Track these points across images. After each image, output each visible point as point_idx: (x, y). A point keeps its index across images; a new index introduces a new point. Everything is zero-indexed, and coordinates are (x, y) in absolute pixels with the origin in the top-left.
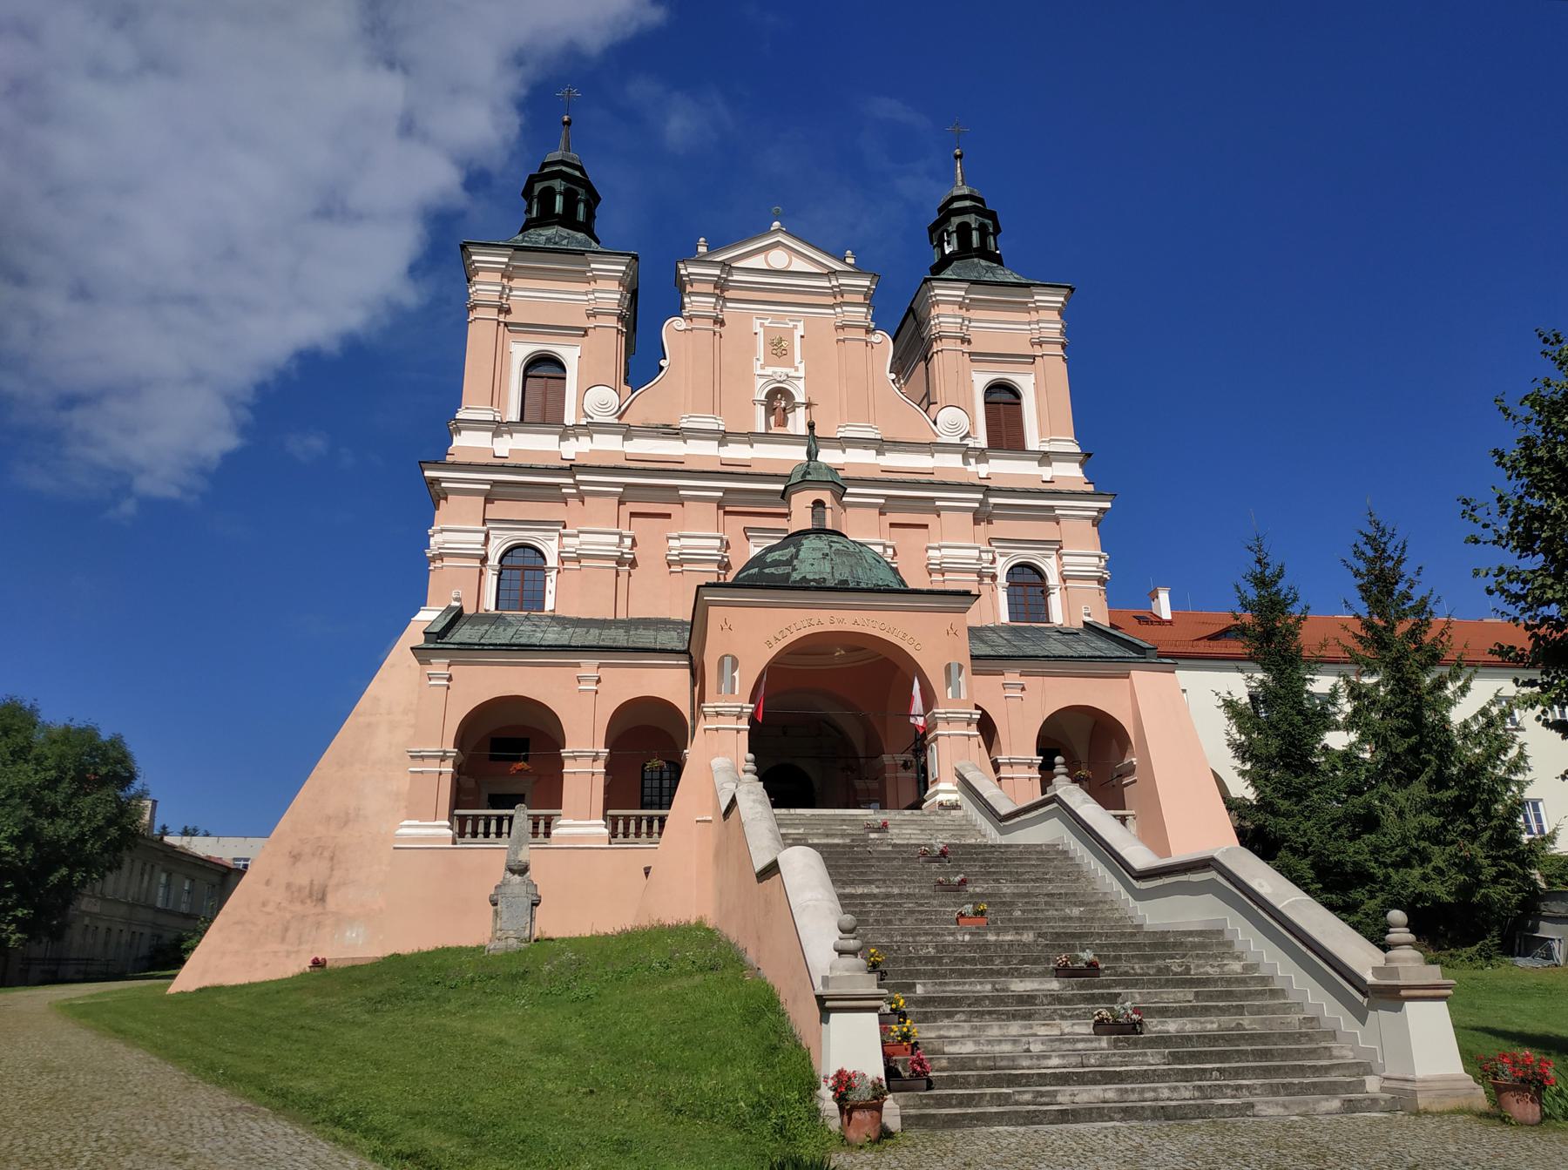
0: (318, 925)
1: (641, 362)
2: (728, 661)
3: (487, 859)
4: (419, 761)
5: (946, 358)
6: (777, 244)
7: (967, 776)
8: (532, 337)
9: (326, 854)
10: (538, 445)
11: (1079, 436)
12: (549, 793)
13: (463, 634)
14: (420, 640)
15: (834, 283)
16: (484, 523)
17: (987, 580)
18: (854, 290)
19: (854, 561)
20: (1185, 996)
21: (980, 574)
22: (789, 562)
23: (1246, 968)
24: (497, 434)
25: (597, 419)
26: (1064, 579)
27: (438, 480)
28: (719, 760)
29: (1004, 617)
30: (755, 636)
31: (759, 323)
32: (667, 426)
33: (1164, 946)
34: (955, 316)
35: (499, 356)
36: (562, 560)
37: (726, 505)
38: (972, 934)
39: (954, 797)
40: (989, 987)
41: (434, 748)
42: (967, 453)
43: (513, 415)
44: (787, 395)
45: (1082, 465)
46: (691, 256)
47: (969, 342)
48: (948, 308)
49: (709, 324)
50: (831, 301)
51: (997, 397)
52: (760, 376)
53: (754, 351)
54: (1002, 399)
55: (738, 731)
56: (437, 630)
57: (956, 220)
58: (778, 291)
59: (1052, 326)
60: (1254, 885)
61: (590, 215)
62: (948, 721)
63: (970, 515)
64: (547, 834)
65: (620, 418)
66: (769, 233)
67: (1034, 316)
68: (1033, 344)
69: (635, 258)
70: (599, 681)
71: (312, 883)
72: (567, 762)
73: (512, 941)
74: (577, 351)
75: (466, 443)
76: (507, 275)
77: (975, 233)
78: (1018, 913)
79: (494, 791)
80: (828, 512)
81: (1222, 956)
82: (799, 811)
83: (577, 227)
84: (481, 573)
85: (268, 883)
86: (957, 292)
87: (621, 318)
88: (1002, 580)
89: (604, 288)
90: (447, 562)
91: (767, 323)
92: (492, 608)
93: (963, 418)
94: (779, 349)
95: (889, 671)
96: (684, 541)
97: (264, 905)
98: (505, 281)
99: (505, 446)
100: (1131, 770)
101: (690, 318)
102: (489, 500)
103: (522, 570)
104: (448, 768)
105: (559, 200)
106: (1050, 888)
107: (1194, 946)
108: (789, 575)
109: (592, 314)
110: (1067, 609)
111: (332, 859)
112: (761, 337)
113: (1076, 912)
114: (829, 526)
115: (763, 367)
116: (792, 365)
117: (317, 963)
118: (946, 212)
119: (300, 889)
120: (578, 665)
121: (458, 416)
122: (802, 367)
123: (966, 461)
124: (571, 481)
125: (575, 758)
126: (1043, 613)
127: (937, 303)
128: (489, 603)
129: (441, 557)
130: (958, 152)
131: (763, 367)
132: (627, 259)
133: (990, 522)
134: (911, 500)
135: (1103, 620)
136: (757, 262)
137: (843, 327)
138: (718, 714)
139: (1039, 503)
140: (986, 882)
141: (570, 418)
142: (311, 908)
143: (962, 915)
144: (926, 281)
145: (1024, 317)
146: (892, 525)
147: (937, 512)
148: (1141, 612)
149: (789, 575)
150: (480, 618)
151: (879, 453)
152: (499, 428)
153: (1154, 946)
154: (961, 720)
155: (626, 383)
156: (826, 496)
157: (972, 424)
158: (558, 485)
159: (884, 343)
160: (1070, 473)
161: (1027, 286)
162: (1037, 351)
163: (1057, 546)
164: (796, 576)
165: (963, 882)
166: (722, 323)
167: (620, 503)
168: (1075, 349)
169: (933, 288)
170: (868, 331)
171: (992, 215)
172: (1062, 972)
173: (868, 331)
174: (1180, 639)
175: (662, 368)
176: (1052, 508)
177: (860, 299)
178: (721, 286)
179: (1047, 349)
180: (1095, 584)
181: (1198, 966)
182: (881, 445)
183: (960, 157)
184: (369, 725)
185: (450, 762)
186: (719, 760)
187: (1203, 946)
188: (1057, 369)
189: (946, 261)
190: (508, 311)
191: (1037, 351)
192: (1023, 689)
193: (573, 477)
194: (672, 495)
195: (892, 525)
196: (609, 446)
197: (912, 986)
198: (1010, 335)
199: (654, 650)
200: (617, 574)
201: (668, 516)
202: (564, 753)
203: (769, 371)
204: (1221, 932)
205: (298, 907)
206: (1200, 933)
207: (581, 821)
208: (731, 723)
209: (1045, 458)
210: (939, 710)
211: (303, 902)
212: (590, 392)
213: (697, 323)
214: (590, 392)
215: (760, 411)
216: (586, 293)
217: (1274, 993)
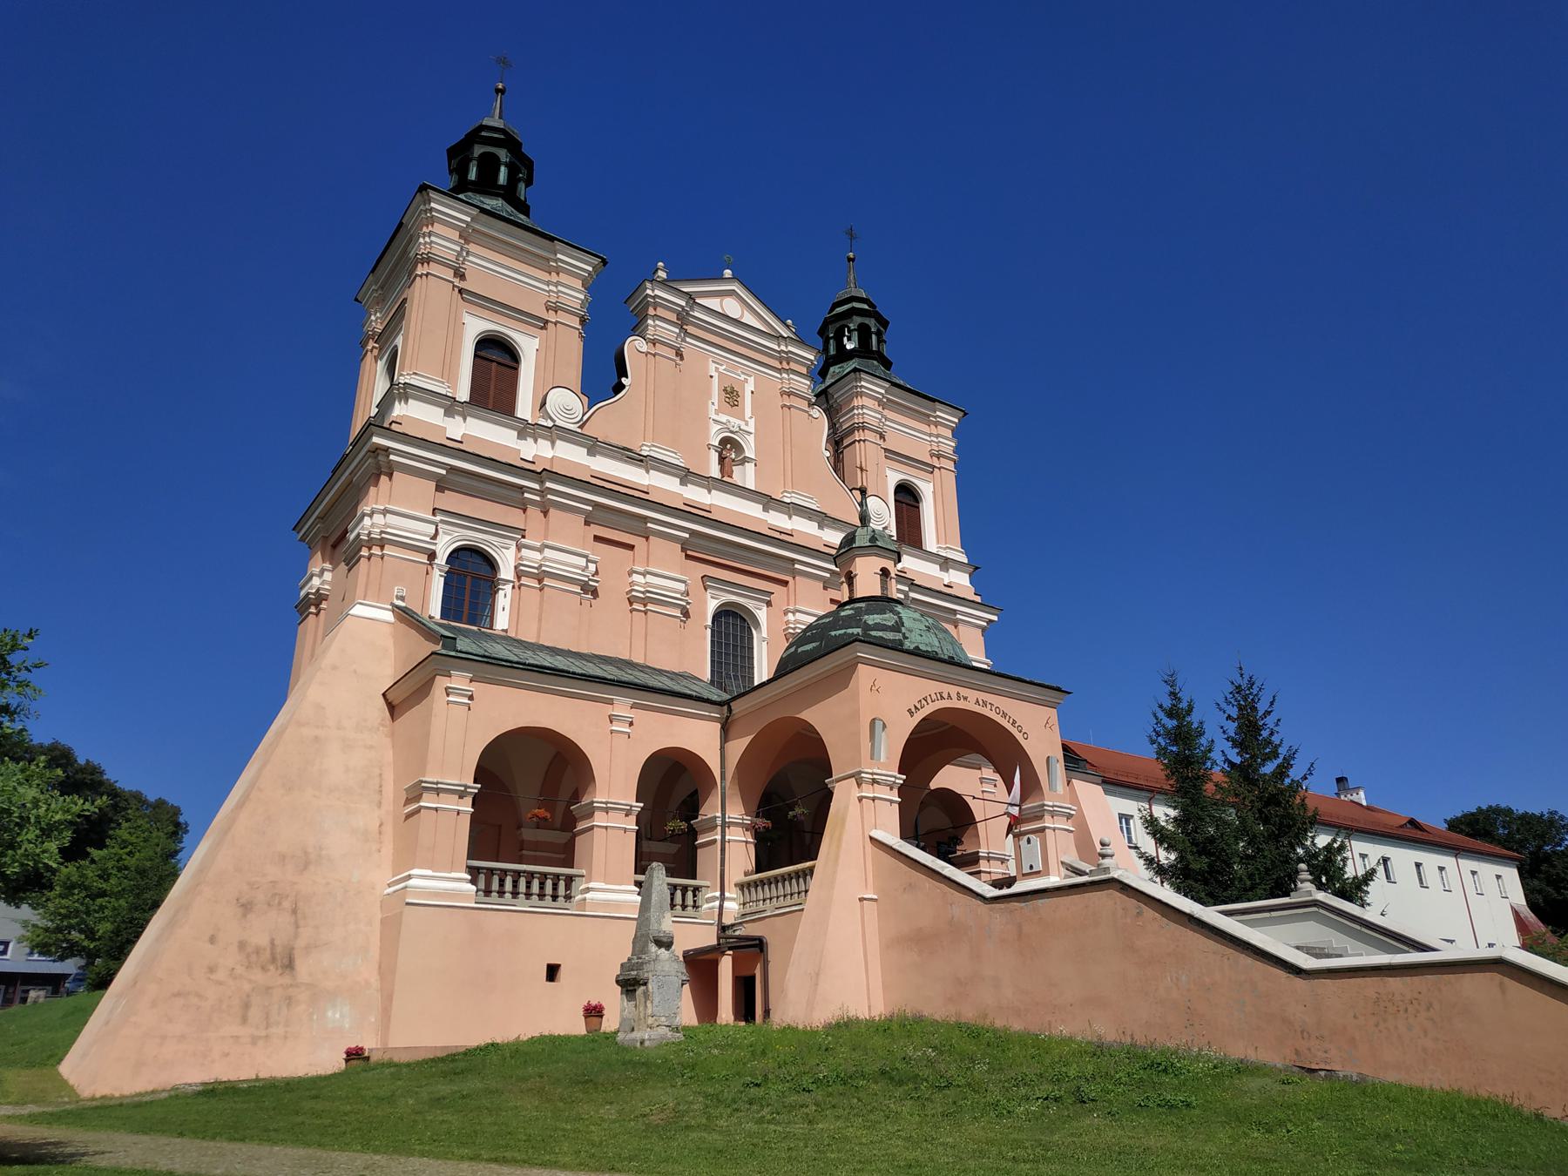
0: (289, 1001)
1: (604, 376)
6: (732, 293)
8: (486, 314)
9: (286, 904)
25: (559, 423)
27: (387, 450)
28: (615, 789)
31: (715, 368)
35: (457, 327)
36: (519, 574)
37: (693, 549)
44: (737, 447)
47: (462, 277)
50: (776, 364)
53: (710, 396)
54: (496, 357)
58: (728, 339)
59: (575, 296)
64: (568, 897)
66: (720, 278)
67: (933, 430)
71: (272, 943)
73: (663, 1031)
85: (212, 940)
86: (463, 216)
89: (565, 283)
91: (721, 369)
94: (732, 396)
96: (650, 578)
97: (212, 970)
101: (654, 342)
111: (294, 912)
112: (716, 379)
117: (354, 1055)
118: (475, 136)
119: (258, 951)
120: (610, 702)
122: (752, 422)
124: (537, 486)
127: (862, 394)
132: (596, 261)
136: (712, 303)
137: (789, 394)
142: (274, 977)
146: (597, 538)
151: (683, 483)
152: (451, 406)
158: (521, 487)
160: (960, 581)
162: (551, 317)
170: (811, 405)
173: (811, 405)
176: (955, 612)
177: (804, 371)
179: (562, 317)
182: (769, 502)
183: (502, 91)
184: (316, 738)
186: (615, 789)
188: (950, 480)
191: (551, 317)
192: (631, 724)
193: (542, 482)
194: (640, 527)
195: (597, 538)
201: (632, 547)
203: (723, 418)
205: (258, 976)
211: (264, 968)
213: (660, 349)
215: (714, 456)
216: (548, 283)
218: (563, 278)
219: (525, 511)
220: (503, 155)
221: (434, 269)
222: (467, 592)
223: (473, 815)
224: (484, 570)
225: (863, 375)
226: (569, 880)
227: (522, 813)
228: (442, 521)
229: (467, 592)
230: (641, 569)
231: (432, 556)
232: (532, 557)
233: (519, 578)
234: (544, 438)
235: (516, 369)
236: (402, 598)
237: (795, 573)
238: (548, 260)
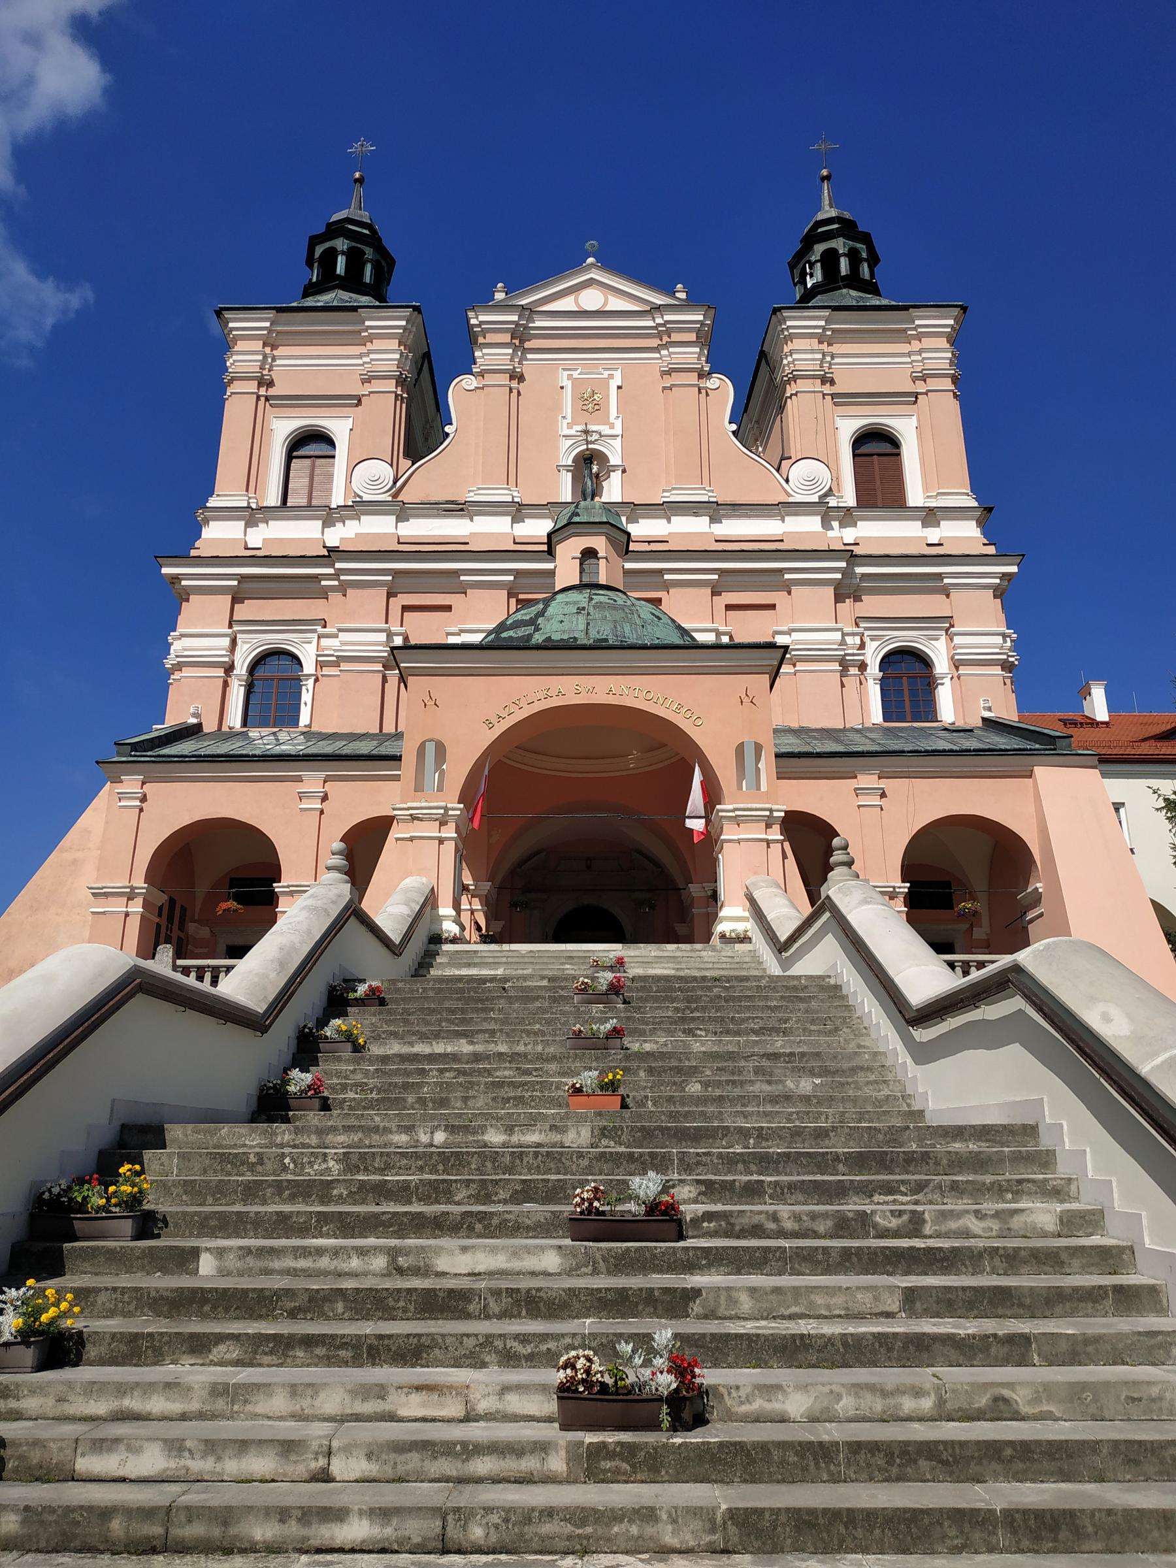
1: (422, 431)
2: (430, 749)
4: (102, 900)
5: (802, 408)
6: (590, 283)
7: (757, 895)
11: (977, 486)
15: (659, 321)
16: (230, 626)
17: (854, 671)
18: (682, 327)
19: (619, 615)
20: (864, 1301)
21: (844, 665)
22: (532, 622)
23: (1072, 1222)
24: (251, 523)
25: (366, 498)
26: (957, 664)
27: (176, 578)
29: (876, 715)
30: (476, 715)
32: (452, 502)
33: (883, 1162)
34: (812, 351)
36: (320, 665)
38: (451, 1129)
39: (740, 927)
40: (379, 1263)
41: (119, 883)
42: (824, 510)
43: (272, 498)
44: (602, 458)
45: (981, 523)
46: (484, 301)
47: (832, 382)
48: (802, 341)
49: (504, 379)
50: (654, 343)
51: (863, 450)
53: (558, 407)
54: (877, 447)
55: (441, 841)
57: (820, 248)
58: (593, 336)
59: (940, 356)
60: (1092, 1018)
62: (738, 821)
63: (830, 591)
65: (395, 495)
67: (916, 345)
68: (914, 380)
69: (416, 308)
70: (325, 798)
72: (282, 900)
74: (349, 423)
75: (218, 534)
76: (270, 342)
78: (694, 1088)
79: (230, 943)
80: (602, 562)
81: (1018, 1189)
82: (514, 947)
83: (362, 289)
84: (226, 684)
87: (401, 381)
88: (874, 669)
89: (380, 346)
90: (187, 672)
91: (576, 374)
93: (821, 466)
94: (590, 403)
95: (671, 759)
98: (268, 350)
99: (259, 537)
100: (1037, 899)
101: (482, 374)
102: (236, 600)
103: (273, 682)
104: (137, 907)
105: (341, 261)
106: (779, 1044)
107: (959, 1163)
108: (530, 636)
109: (367, 380)
110: (960, 702)
113: (806, 1085)
114: (602, 580)
115: (570, 426)
118: (811, 239)
120: (299, 779)
121: (208, 505)
122: (618, 424)
123: (826, 525)
124: (331, 571)
125: (291, 893)
126: (926, 708)
127: (791, 337)
128: (234, 718)
129: (179, 667)
130: (825, 172)
131: (570, 426)
132: (407, 312)
133: (857, 599)
134: (752, 574)
135: (1008, 712)
136: (566, 304)
137: (669, 372)
138: (414, 818)
139: (923, 573)
140: (670, 1032)
143: (578, 1091)
144: (775, 311)
145: (904, 348)
146: (729, 607)
147: (787, 587)
148: (1070, 715)
149: (530, 636)
150: (232, 735)
152: (253, 516)
153: (859, 1161)
154: (756, 819)
155: (407, 455)
156: (599, 543)
157: (836, 479)
159: (723, 390)
160: (965, 533)
161: (905, 308)
162: (920, 387)
163: (945, 624)
164: (538, 638)
165: (617, 1033)
166: (521, 378)
167: (390, 595)
168: (969, 383)
169: (785, 320)
170: (702, 375)
171: (866, 238)
172: (593, 1225)
173: (702, 375)
174: (1120, 741)
175: (447, 435)
176: (939, 577)
177: (507, 338)
178: (520, 337)
179: (933, 384)
180: (997, 670)
181: (944, 1215)
182: (716, 510)
183: (828, 178)
184: (74, 862)
185: (139, 901)
187: (979, 1163)
188: (946, 409)
189: (808, 296)
190: (271, 384)
191: (920, 387)
192: (883, 795)
193: (333, 566)
194: (776, 581)
196: (379, 528)
197: (186, 1259)
198: (890, 373)
200: (385, 680)
201: (448, 608)
202: (278, 887)
204: (1030, 1131)
206: (984, 1132)
208: (432, 830)
209: (930, 516)
210: (725, 808)
213: (490, 379)
214: (361, 466)
215: (567, 478)
216: (360, 356)
217: (1129, 1299)
218: (927, 343)
219: (789, 593)
220: (369, 252)
221: (802, 386)
222: (906, 693)
223: (907, 914)
224: (918, 668)
225: (786, 314)
228: (867, 629)
229: (906, 693)
230: (785, 628)
233: (957, 668)
234: (351, 518)
235: (899, 454)
236: (989, 709)
237: (667, 586)
238: (360, 332)
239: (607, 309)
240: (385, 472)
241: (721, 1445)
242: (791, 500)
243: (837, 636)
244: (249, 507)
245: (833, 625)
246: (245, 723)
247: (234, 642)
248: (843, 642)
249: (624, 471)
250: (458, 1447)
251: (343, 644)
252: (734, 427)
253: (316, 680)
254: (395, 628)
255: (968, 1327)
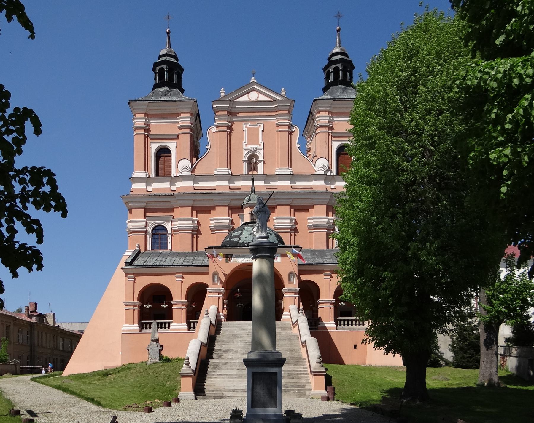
3: (148, 335)
10: (161, 186)
12: (168, 314)
13: (139, 262)
14: (124, 265)
22: (239, 237)
25: (184, 173)
28: (179, 297)
43: (153, 173)
52: (245, 150)
53: (242, 138)
56: (129, 261)
57: (333, 66)
61: (180, 78)
64: (169, 328)
77: (340, 72)
92: (150, 249)
116: (258, 143)
128: (149, 248)
131: (246, 145)
141: (173, 174)
149: (238, 241)
152: (148, 180)
177: (225, 113)
186: (179, 297)
199: (200, 266)
207: (178, 325)
212: (180, 165)
226: (169, 323)
227: (153, 306)
231: (146, 232)
232: (176, 224)
239: (259, 100)
240: (188, 163)
241: (338, 85)
242: (316, 173)
243: (327, 220)
244: (146, 177)
245: (326, 217)
246: (152, 249)
247: (147, 223)
248: (328, 222)
249: (264, 162)
250: (165, 306)
251: (180, 224)
252: (299, 145)
253: (172, 236)
254: (195, 218)
255: (55, 341)
